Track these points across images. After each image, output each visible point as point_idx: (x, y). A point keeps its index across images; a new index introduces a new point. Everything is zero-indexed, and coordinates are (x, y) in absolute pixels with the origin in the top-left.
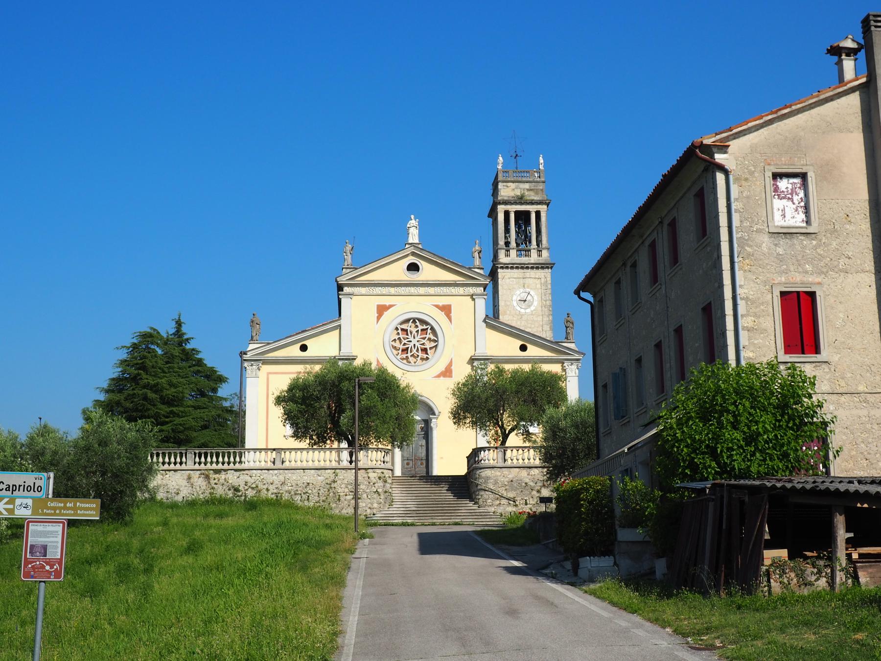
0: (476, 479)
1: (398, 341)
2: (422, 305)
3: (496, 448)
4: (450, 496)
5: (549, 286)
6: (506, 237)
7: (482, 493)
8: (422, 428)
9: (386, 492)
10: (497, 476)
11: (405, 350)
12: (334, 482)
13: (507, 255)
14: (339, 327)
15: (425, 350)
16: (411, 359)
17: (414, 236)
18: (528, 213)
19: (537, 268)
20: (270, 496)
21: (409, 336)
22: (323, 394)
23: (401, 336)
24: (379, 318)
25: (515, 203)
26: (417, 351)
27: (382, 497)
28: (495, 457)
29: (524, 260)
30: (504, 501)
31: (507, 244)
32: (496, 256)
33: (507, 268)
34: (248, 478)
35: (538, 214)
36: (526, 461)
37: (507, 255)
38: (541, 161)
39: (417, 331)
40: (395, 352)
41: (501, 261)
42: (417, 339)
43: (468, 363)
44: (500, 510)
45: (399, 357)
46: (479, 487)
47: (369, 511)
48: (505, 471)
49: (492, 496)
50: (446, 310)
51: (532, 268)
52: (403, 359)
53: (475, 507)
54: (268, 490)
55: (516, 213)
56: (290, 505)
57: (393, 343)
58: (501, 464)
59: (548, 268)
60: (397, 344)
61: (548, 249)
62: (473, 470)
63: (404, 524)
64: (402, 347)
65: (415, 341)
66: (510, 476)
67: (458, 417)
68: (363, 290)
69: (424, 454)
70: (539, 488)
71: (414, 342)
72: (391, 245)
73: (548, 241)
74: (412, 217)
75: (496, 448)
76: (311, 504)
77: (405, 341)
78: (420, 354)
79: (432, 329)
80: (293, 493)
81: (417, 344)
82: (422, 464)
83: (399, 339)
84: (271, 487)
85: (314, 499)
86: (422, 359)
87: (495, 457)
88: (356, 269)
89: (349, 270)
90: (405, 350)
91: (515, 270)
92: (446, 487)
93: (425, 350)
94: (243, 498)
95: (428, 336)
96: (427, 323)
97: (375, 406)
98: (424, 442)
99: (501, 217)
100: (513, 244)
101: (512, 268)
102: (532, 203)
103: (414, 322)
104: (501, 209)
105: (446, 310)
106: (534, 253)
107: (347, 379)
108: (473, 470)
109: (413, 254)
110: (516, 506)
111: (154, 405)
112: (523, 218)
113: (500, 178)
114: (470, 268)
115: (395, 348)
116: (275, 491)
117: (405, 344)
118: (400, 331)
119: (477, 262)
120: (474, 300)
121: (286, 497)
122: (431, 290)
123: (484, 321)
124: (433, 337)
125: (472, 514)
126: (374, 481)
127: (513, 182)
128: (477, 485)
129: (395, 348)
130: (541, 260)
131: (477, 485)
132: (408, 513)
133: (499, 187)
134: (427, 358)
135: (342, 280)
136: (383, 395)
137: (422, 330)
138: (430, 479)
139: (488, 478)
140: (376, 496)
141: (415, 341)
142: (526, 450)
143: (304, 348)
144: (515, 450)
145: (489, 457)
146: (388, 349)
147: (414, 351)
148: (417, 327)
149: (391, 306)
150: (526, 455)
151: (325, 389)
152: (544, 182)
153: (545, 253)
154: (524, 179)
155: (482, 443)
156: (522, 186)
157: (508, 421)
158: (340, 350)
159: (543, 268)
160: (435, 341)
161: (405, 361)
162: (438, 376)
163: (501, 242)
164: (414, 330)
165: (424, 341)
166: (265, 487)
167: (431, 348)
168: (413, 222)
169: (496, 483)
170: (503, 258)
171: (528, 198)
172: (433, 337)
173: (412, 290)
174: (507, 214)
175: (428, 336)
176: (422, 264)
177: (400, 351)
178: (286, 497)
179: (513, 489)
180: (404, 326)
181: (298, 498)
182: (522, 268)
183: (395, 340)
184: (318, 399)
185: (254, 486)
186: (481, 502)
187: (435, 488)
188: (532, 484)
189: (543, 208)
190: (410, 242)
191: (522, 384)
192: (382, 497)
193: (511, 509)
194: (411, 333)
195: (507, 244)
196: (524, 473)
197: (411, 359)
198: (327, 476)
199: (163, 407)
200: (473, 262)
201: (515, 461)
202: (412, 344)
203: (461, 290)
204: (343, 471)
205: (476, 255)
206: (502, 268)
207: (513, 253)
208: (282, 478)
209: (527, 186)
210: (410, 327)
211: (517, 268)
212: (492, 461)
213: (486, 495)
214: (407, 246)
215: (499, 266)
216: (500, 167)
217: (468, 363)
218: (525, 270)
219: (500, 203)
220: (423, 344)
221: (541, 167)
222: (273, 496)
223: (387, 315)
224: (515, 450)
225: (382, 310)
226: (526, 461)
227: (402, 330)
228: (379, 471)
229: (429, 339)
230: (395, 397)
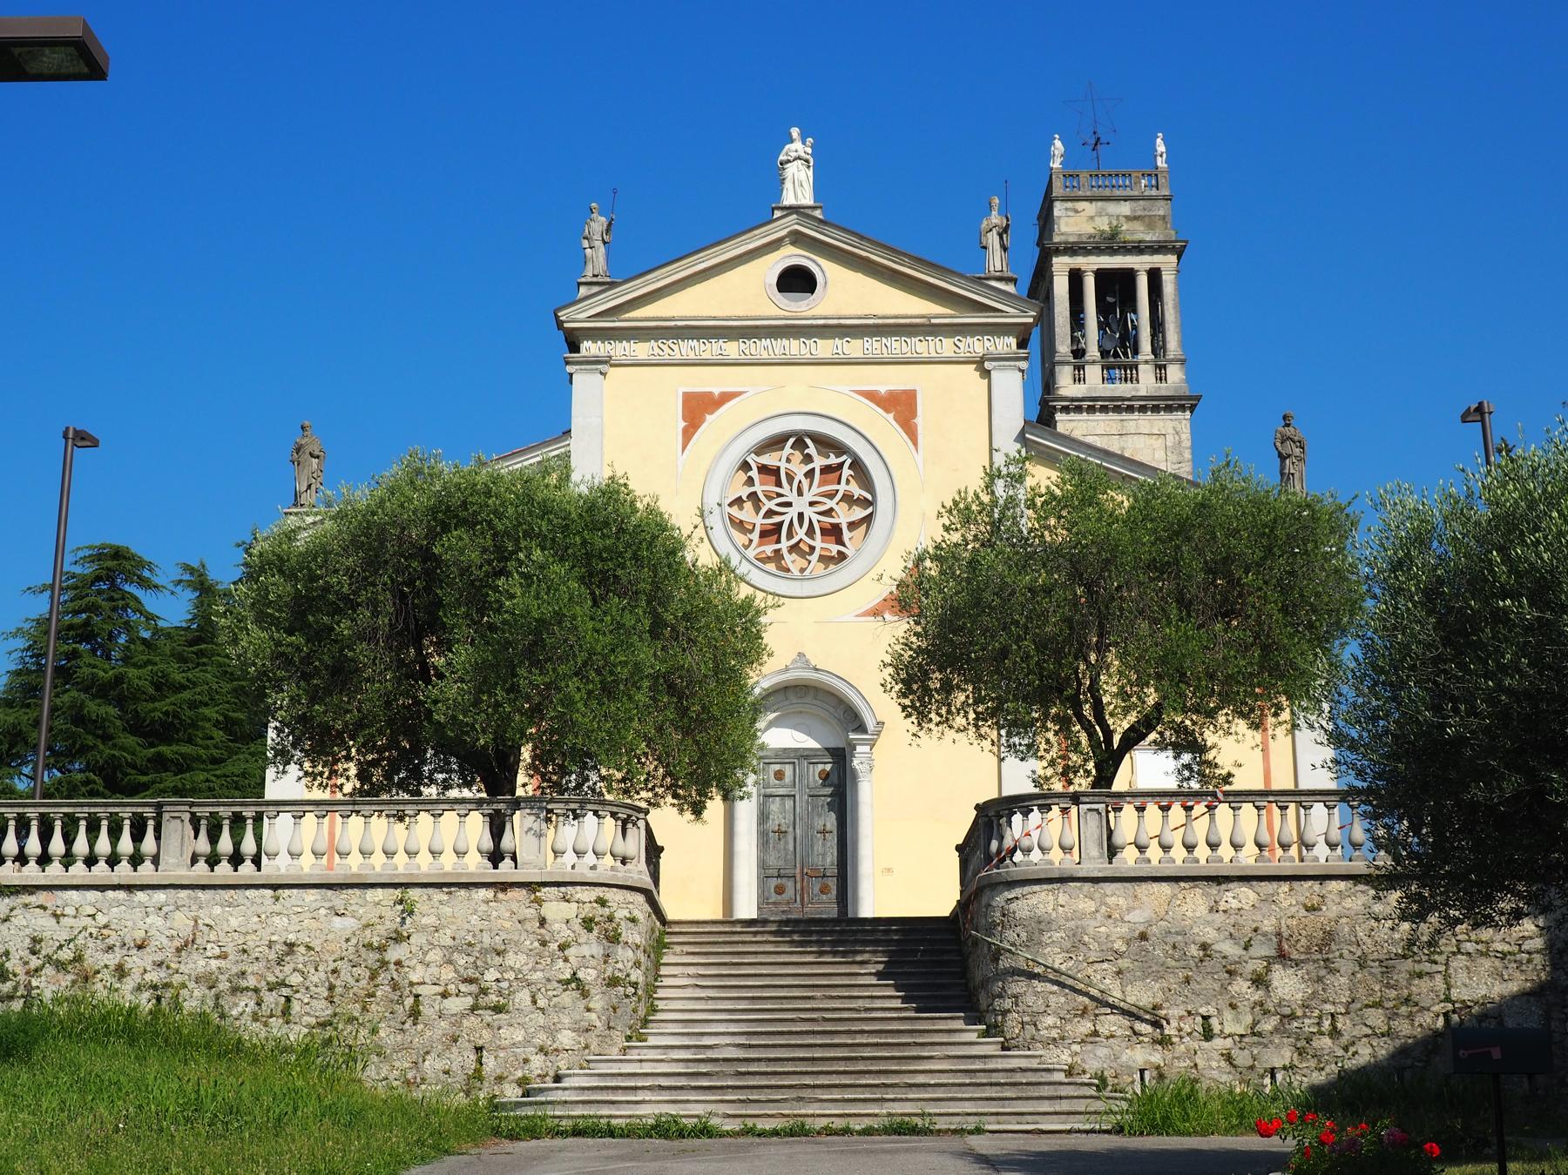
0: (990, 929)
1: (748, 505)
2: (826, 394)
3: (1076, 798)
4: (889, 999)
5: (1187, 455)
6: (1074, 340)
7: (1018, 986)
9: (613, 982)
10: (1082, 916)
11: (771, 533)
12: (398, 938)
13: (1078, 379)
15: (834, 532)
16: (789, 559)
17: (799, 186)
18: (1129, 276)
19: (1156, 409)
20: (126, 995)
21: (785, 489)
22: (366, 583)
23: (758, 488)
24: (688, 434)
25: (1097, 250)
26: (810, 532)
27: (597, 1002)
28: (1072, 837)
29: (1122, 389)
30: (1112, 1023)
31: (1079, 353)
32: (1049, 384)
33: (1078, 409)
34: (42, 923)
35: (1155, 276)
36: (1202, 852)
37: (1078, 379)
38: (1161, 147)
39: (810, 474)
40: (740, 539)
41: (1063, 392)
42: (809, 496)
44: (1096, 1060)
45: (751, 553)
46: (1005, 963)
47: (537, 1062)
48: (1116, 896)
49: (1059, 999)
50: (902, 406)
51: (1143, 409)
52: (767, 560)
53: (990, 1047)
54: (121, 972)
55: (1100, 275)
56: (210, 1041)
57: (734, 511)
58: (1095, 864)
59: (1182, 408)
60: (747, 514)
61: (1183, 362)
62: (979, 891)
63: (663, 1130)
64: (759, 521)
65: (802, 504)
66: (1137, 917)
67: (920, 684)
68: (642, 350)
69: (831, 857)
70: (1259, 966)
71: (800, 505)
72: (730, 208)
73: (1183, 343)
74: (795, 132)
75: (1076, 798)
76: (296, 1034)
77: (771, 505)
78: (818, 542)
79: (858, 465)
80: (224, 986)
81: (809, 513)
82: (824, 890)
83: (753, 496)
84: (136, 962)
85: (311, 1009)
86: (826, 560)
87: (1072, 837)
88: (612, 285)
89: (596, 289)
90: (771, 533)
91: (1098, 416)
92: (875, 961)
93: (834, 532)
94: (17, 1005)
95: (842, 488)
96: (838, 447)
97: (559, 617)
98: (831, 821)
99: (1061, 286)
100: (1093, 352)
101: (1091, 410)
102: (1139, 249)
103: (800, 444)
104: (1061, 266)
105: (902, 406)
106: (1146, 374)
107: (462, 522)
108: (979, 891)
109: (797, 239)
110: (1164, 1042)
111: (106, 738)
112: (1117, 287)
113: (1058, 190)
114: (979, 281)
115: (740, 525)
116: (154, 976)
117: (770, 513)
118: (754, 473)
119: (996, 261)
120: (986, 374)
121: (194, 1000)
122: (854, 347)
124: (857, 491)
125: (976, 1078)
126: (565, 934)
127: (1090, 199)
128: (997, 954)
129: (740, 525)
130: (1164, 389)
131: (997, 954)
132: (702, 1074)
133: (1056, 213)
134: (842, 556)
135: (577, 317)
136: (600, 577)
137: (826, 470)
138: (843, 932)
139: (1041, 924)
140: (568, 997)
141: (802, 504)
142: (1200, 808)
144: (1152, 809)
145: (1044, 838)
146: (715, 521)
147: (800, 533)
149: (726, 397)
150: (1200, 828)
151: (374, 563)
152: (1167, 199)
153: (1175, 374)
154: (1118, 193)
155: (1019, 777)
156: (1112, 208)
157: (1115, 690)
159: (1169, 409)
160: (866, 503)
161: (771, 567)
163: (1063, 347)
164: (800, 471)
165: (830, 504)
166: (112, 960)
167: (853, 526)
168: (798, 147)
169: (1076, 943)
170: (1067, 386)
171: (1128, 238)
172: (857, 491)
173: (795, 347)
174: (1076, 277)
175: (842, 488)
176: (827, 271)
177: (755, 536)
178: (194, 1000)
179: (1151, 971)
180: (769, 459)
181: (245, 1004)
182: (1117, 409)
183: (738, 502)
184: (349, 604)
185: (66, 955)
186: (1012, 1025)
187: (832, 968)
188: (1230, 949)
189: (1166, 262)
190: (786, 203)
191: (1181, 530)
192: (597, 1002)
193: (1141, 1055)
194: (790, 479)
195: (1079, 353)
196: (1195, 902)
197: (789, 559)
198: (370, 914)
199: (131, 740)
200: (983, 261)
201: (1154, 853)
202: (792, 513)
203: (946, 346)
204: (438, 895)
205: (993, 240)
206: (1066, 410)
207: (1094, 373)
208: (182, 923)
209: (1125, 208)
210: (785, 459)
211: (1104, 409)
212: (1056, 855)
213: (1034, 995)
214: (778, 214)
215: (1059, 404)
216: (1056, 164)
218: (1125, 416)
219: (1058, 252)
220: (829, 513)
221: (1161, 163)
222: (145, 1001)
223: (715, 425)
224: (1152, 809)
225: (697, 408)
226: (1202, 852)
227: (763, 469)
228: (589, 894)
229: (848, 499)
230: (657, 597)
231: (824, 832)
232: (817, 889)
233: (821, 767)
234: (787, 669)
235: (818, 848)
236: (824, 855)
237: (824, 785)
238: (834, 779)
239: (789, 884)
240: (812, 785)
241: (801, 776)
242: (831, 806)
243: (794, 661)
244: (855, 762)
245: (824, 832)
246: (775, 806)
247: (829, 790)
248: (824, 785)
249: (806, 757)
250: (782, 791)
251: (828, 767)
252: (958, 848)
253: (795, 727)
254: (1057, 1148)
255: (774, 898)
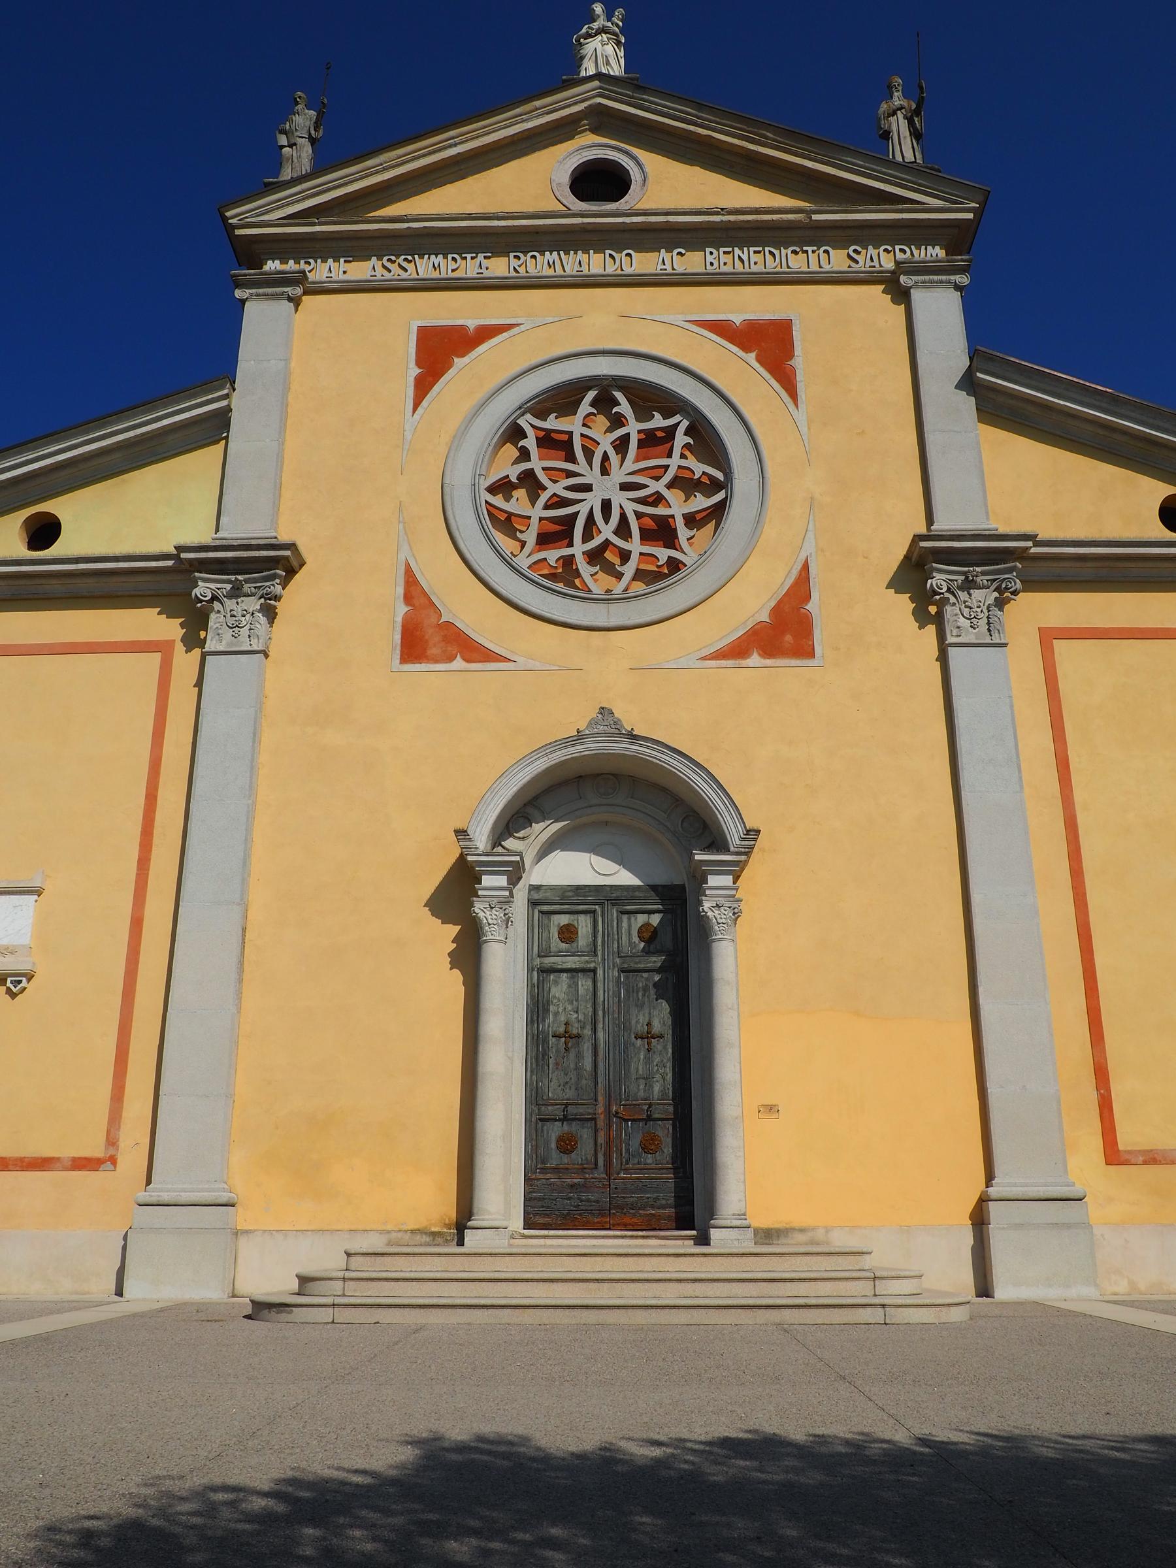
8: (650, 936)
14: (227, 438)
21: (581, 466)
23: (536, 464)
24: (423, 387)
26: (623, 530)
40: (506, 544)
43: (897, 583)
50: (771, 344)
69: (661, 1083)
71: (605, 488)
74: (598, 8)
77: (558, 488)
82: (649, 1145)
96: (669, 403)
98: (660, 1016)
103: (604, 403)
105: (771, 344)
117: (558, 502)
120: (901, 295)
123: (968, 383)
134: (674, 566)
143: (44, 532)
147: (606, 531)
148: (618, 421)
149: (486, 333)
158: (990, 1177)
162: (737, 651)
167: (691, 520)
172: (699, 468)
217: (897, 583)
223: (467, 375)
225: (438, 351)
227: (547, 441)
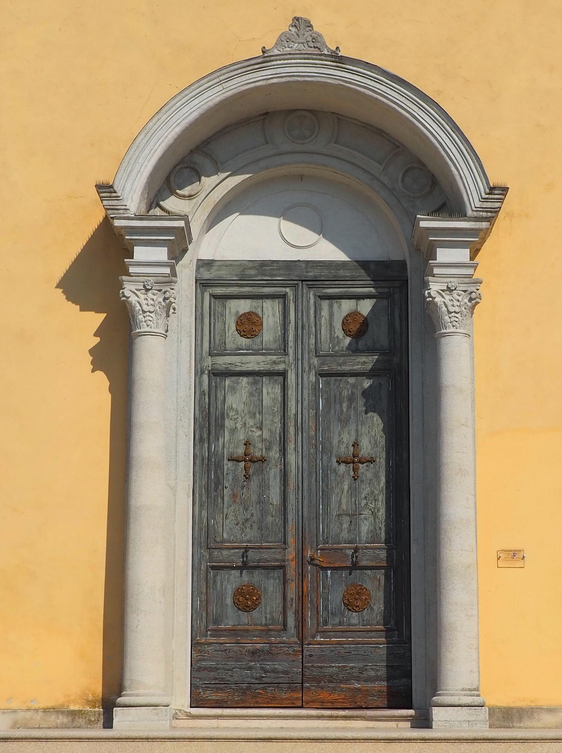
82: (354, 601)
98: (370, 434)
172: (365, 674)
231: (354, 460)
232: (336, 598)
233: (347, 306)
234: (266, 58)
235: (340, 498)
236: (354, 516)
237: (354, 350)
238: (380, 334)
239: (270, 586)
240: (325, 347)
241: (300, 327)
242: (371, 401)
243: (284, 39)
244: (435, 287)
245: (354, 460)
246: (237, 398)
247: (367, 362)
248: (354, 350)
249: (313, 283)
250: (254, 363)
251: (366, 307)
252: (81, 310)
253: (287, 213)
254: (195, 115)
255: (232, 618)
